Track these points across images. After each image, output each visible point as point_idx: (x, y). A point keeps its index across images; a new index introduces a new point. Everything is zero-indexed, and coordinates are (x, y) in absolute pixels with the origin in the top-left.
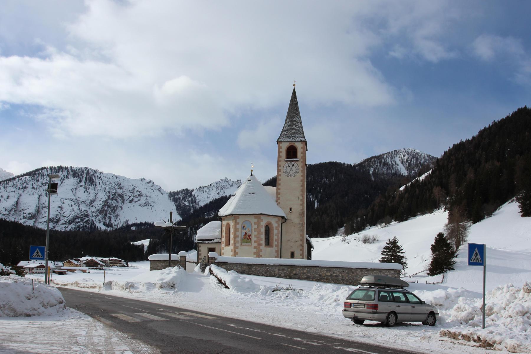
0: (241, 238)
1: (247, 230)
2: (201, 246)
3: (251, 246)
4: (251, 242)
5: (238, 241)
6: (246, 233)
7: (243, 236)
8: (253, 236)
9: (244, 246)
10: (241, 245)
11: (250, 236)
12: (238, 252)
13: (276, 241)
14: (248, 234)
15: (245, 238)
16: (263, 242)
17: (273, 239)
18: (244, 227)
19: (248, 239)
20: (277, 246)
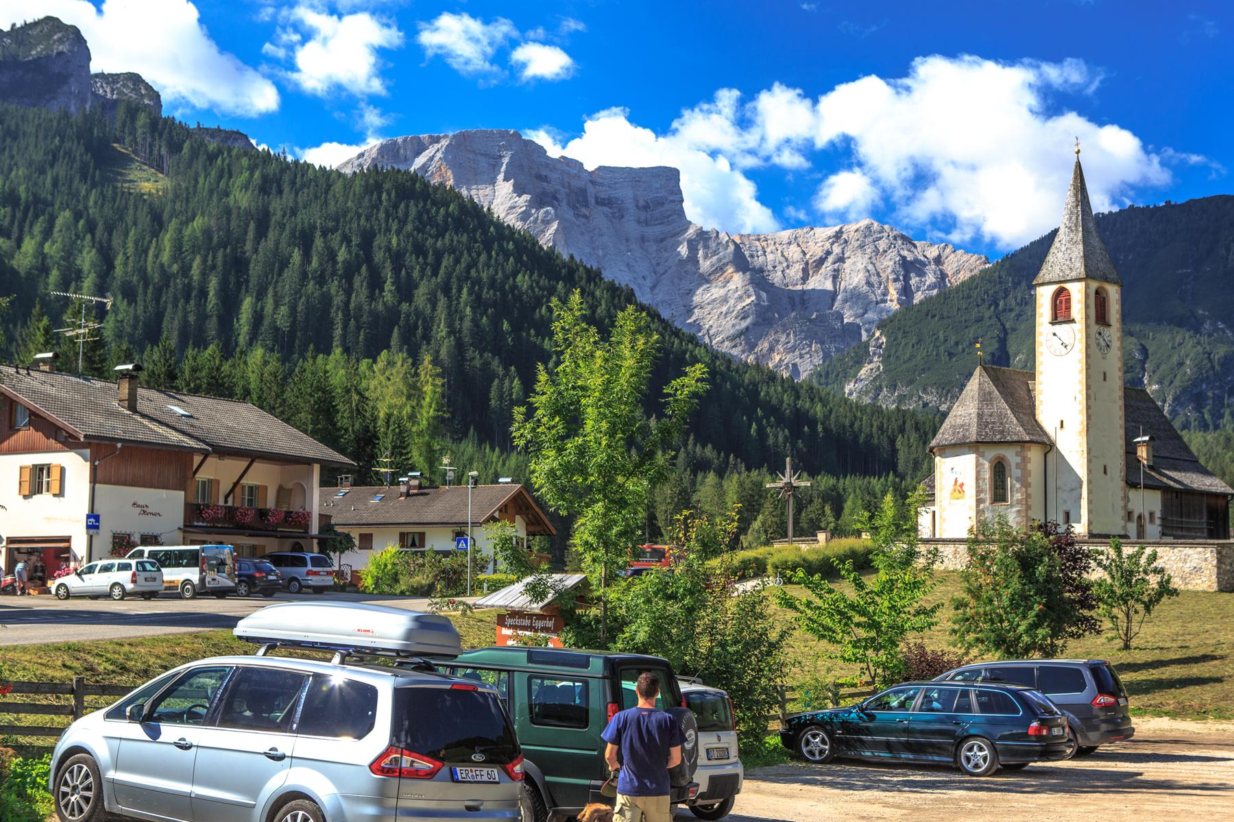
11: (962, 485)
14: (959, 483)
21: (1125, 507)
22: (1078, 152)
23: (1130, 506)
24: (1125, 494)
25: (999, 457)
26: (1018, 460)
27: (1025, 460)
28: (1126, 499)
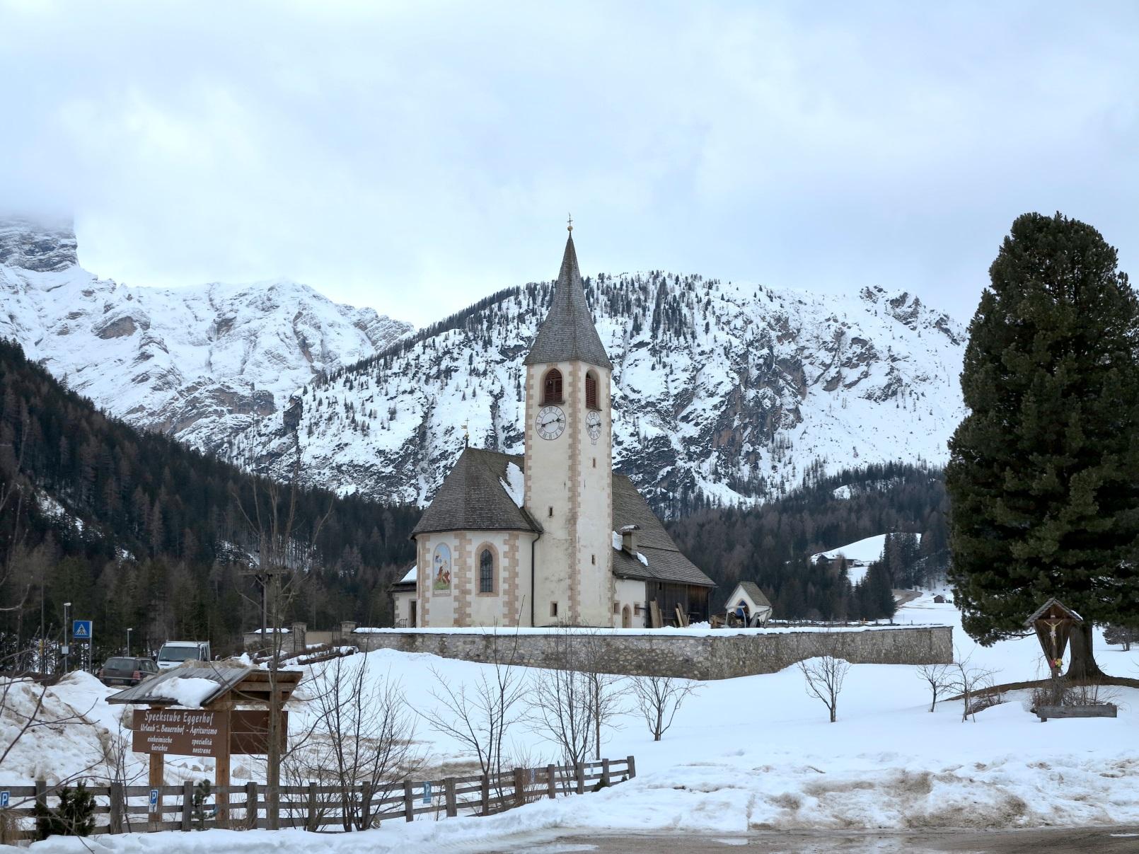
0: (433, 580)
1: (443, 564)
2: (398, 599)
3: (450, 595)
4: (448, 587)
5: (428, 587)
6: (441, 569)
7: (436, 576)
8: (453, 576)
9: (437, 596)
10: (434, 595)
11: (447, 574)
12: (428, 610)
13: (504, 582)
14: (444, 572)
15: (439, 580)
16: (473, 586)
17: (498, 580)
18: (437, 557)
19: (444, 581)
20: (505, 592)
21: (612, 598)
22: (570, 229)
23: (617, 597)
24: (611, 585)
25: (486, 545)
26: (506, 548)
27: (514, 549)
28: (613, 590)
